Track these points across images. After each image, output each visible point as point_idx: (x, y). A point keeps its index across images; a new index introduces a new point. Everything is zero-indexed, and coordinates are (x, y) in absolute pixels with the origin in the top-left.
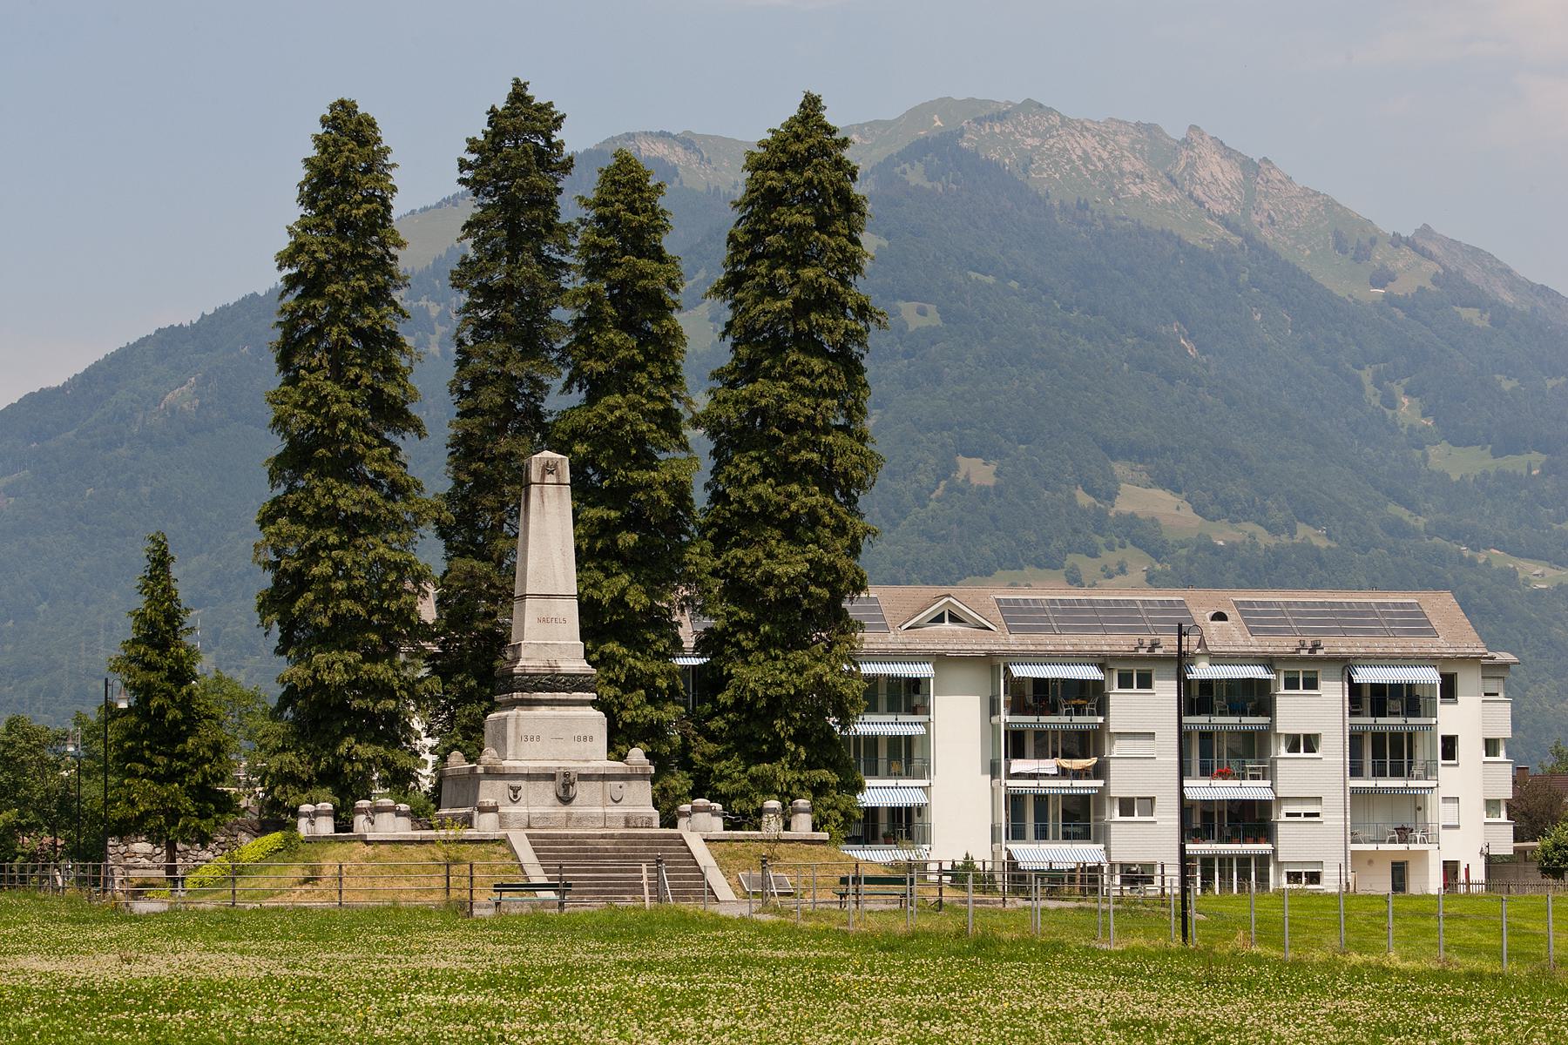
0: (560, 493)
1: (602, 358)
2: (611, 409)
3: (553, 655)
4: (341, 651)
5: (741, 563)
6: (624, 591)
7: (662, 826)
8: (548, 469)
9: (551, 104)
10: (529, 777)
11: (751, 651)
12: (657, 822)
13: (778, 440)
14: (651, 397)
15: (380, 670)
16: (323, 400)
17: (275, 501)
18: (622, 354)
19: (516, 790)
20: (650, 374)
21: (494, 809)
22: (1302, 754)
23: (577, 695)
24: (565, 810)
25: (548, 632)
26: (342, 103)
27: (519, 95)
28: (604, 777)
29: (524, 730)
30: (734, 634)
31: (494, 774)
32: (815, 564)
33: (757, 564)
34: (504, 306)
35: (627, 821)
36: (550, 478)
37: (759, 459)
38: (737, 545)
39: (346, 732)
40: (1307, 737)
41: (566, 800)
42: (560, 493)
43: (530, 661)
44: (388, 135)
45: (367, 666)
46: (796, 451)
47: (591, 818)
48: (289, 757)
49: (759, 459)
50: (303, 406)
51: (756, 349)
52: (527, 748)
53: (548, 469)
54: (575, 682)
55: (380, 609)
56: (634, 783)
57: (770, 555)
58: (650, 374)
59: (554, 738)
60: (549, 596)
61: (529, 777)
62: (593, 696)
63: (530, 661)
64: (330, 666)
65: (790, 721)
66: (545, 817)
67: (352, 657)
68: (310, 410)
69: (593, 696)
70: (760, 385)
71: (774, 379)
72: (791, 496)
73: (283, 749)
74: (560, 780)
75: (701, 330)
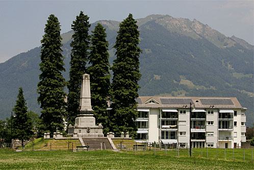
1: (95, 58)
3: (86, 108)
6: (98, 97)
8: (86, 77)
10: (82, 128)
14: (103, 65)
15: (58, 110)
16: (49, 65)
25: (86, 104)
28: (95, 128)
33: (121, 92)
39: (52, 121)
43: (83, 109)
46: (127, 74)
48: (43, 125)
51: (121, 56)
52: (82, 124)
54: (90, 112)
55: (58, 100)
57: (123, 91)
59: (86, 121)
61: (82, 128)
63: (83, 109)
66: (85, 135)
67: (53, 108)
75: (112, 53)
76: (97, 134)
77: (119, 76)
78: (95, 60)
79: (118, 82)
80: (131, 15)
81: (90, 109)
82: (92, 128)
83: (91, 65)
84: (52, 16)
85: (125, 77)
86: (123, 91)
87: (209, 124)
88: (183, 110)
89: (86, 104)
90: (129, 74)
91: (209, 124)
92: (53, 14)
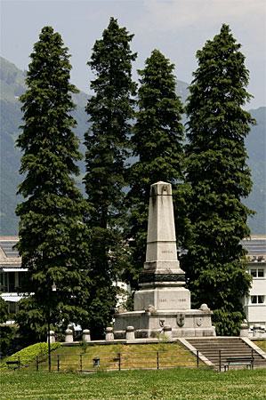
0: (169, 200)
1: (155, 142)
2: (160, 163)
4: (58, 266)
5: (204, 226)
7: (217, 335)
8: (164, 189)
9: (125, 28)
10: (167, 316)
11: (207, 264)
12: (215, 334)
13: (217, 175)
14: (174, 158)
16: (50, 160)
17: (24, 204)
18: (163, 139)
19: (162, 322)
20: (173, 148)
21: (170, 329)
22: (258, 304)
23: (178, 283)
24: (180, 329)
25: (166, 256)
26: (47, 29)
27: (113, 25)
28: (194, 316)
29: (160, 297)
30: (199, 256)
31: (155, 315)
32: (237, 227)
33: (211, 227)
34: (106, 116)
35: (204, 333)
36: (165, 193)
37: (209, 183)
38: (202, 220)
39: (59, 301)
40: (259, 297)
41: (181, 326)
42: (169, 200)
43: (160, 269)
44: (66, 42)
45: (69, 273)
46: (225, 180)
47: (190, 333)
48: (35, 311)
49: (209, 183)
50: (41, 163)
51: (202, 140)
53: (164, 189)
54: (177, 277)
55: (75, 248)
56: (205, 318)
57: (216, 223)
58: (173, 148)
59: (174, 299)
60: (165, 242)
61: (167, 316)
62: (184, 283)
63: (160, 269)
64: (55, 273)
65: (226, 292)
67: (64, 269)
68: (44, 164)
69: (184, 283)
70: (209, 152)
71: (214, 149)
72: (223, 199)
73: (33, 308)
74: (179, 317)
75: (81, 125)
76: (198, 329)
77: (204, 185)
78: (154, 145)
79: (203, 202)
80: (227, 27)
81: (178, 270)
82: (187, 316)
83: (137, 159)
84: (48, 30)
85: (220, 189)
86: (216, 223)
87: (254, 302)
88: (257, 269)
89: (166, 256)
90: (230, 180)
91: (254, 302)
92: (49, 25)
